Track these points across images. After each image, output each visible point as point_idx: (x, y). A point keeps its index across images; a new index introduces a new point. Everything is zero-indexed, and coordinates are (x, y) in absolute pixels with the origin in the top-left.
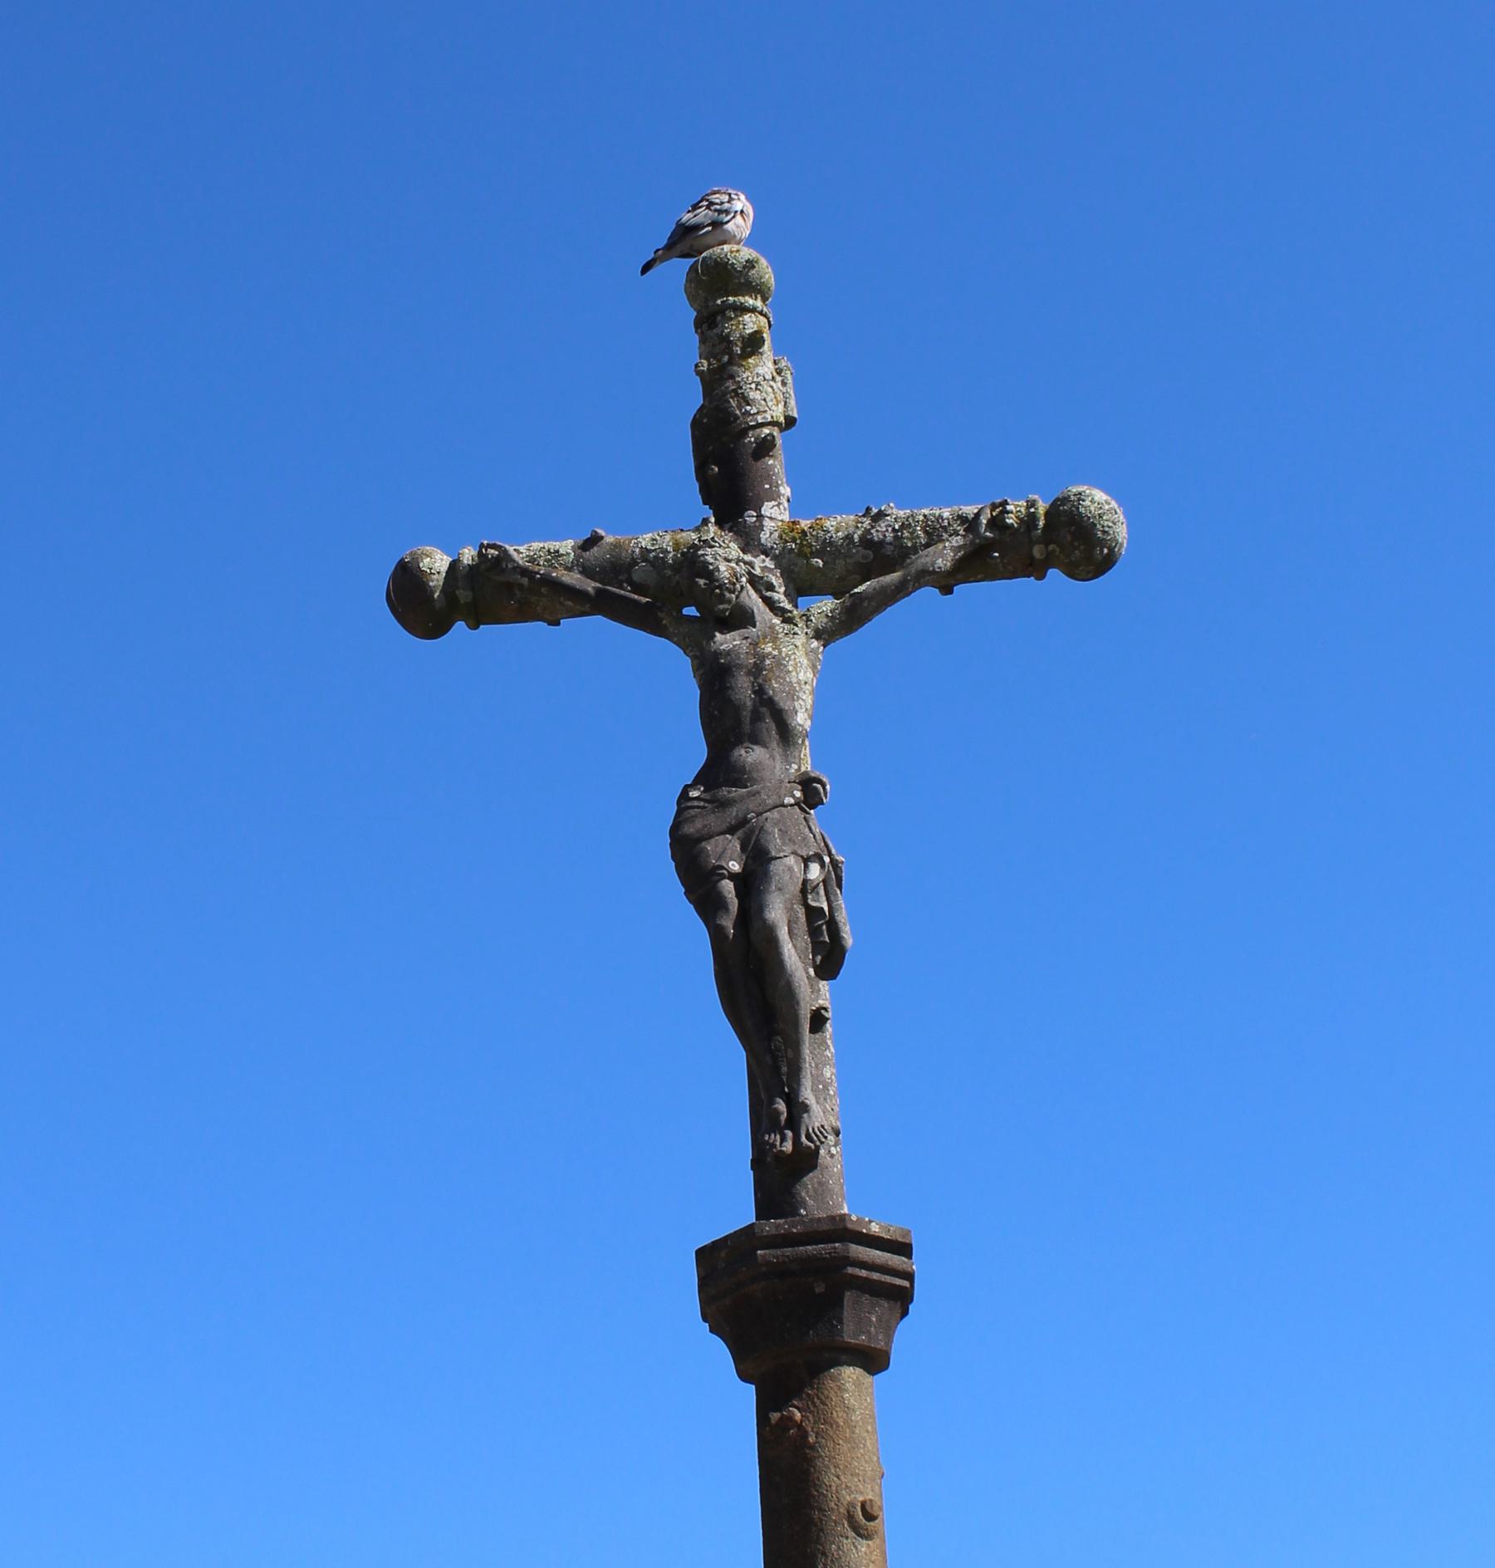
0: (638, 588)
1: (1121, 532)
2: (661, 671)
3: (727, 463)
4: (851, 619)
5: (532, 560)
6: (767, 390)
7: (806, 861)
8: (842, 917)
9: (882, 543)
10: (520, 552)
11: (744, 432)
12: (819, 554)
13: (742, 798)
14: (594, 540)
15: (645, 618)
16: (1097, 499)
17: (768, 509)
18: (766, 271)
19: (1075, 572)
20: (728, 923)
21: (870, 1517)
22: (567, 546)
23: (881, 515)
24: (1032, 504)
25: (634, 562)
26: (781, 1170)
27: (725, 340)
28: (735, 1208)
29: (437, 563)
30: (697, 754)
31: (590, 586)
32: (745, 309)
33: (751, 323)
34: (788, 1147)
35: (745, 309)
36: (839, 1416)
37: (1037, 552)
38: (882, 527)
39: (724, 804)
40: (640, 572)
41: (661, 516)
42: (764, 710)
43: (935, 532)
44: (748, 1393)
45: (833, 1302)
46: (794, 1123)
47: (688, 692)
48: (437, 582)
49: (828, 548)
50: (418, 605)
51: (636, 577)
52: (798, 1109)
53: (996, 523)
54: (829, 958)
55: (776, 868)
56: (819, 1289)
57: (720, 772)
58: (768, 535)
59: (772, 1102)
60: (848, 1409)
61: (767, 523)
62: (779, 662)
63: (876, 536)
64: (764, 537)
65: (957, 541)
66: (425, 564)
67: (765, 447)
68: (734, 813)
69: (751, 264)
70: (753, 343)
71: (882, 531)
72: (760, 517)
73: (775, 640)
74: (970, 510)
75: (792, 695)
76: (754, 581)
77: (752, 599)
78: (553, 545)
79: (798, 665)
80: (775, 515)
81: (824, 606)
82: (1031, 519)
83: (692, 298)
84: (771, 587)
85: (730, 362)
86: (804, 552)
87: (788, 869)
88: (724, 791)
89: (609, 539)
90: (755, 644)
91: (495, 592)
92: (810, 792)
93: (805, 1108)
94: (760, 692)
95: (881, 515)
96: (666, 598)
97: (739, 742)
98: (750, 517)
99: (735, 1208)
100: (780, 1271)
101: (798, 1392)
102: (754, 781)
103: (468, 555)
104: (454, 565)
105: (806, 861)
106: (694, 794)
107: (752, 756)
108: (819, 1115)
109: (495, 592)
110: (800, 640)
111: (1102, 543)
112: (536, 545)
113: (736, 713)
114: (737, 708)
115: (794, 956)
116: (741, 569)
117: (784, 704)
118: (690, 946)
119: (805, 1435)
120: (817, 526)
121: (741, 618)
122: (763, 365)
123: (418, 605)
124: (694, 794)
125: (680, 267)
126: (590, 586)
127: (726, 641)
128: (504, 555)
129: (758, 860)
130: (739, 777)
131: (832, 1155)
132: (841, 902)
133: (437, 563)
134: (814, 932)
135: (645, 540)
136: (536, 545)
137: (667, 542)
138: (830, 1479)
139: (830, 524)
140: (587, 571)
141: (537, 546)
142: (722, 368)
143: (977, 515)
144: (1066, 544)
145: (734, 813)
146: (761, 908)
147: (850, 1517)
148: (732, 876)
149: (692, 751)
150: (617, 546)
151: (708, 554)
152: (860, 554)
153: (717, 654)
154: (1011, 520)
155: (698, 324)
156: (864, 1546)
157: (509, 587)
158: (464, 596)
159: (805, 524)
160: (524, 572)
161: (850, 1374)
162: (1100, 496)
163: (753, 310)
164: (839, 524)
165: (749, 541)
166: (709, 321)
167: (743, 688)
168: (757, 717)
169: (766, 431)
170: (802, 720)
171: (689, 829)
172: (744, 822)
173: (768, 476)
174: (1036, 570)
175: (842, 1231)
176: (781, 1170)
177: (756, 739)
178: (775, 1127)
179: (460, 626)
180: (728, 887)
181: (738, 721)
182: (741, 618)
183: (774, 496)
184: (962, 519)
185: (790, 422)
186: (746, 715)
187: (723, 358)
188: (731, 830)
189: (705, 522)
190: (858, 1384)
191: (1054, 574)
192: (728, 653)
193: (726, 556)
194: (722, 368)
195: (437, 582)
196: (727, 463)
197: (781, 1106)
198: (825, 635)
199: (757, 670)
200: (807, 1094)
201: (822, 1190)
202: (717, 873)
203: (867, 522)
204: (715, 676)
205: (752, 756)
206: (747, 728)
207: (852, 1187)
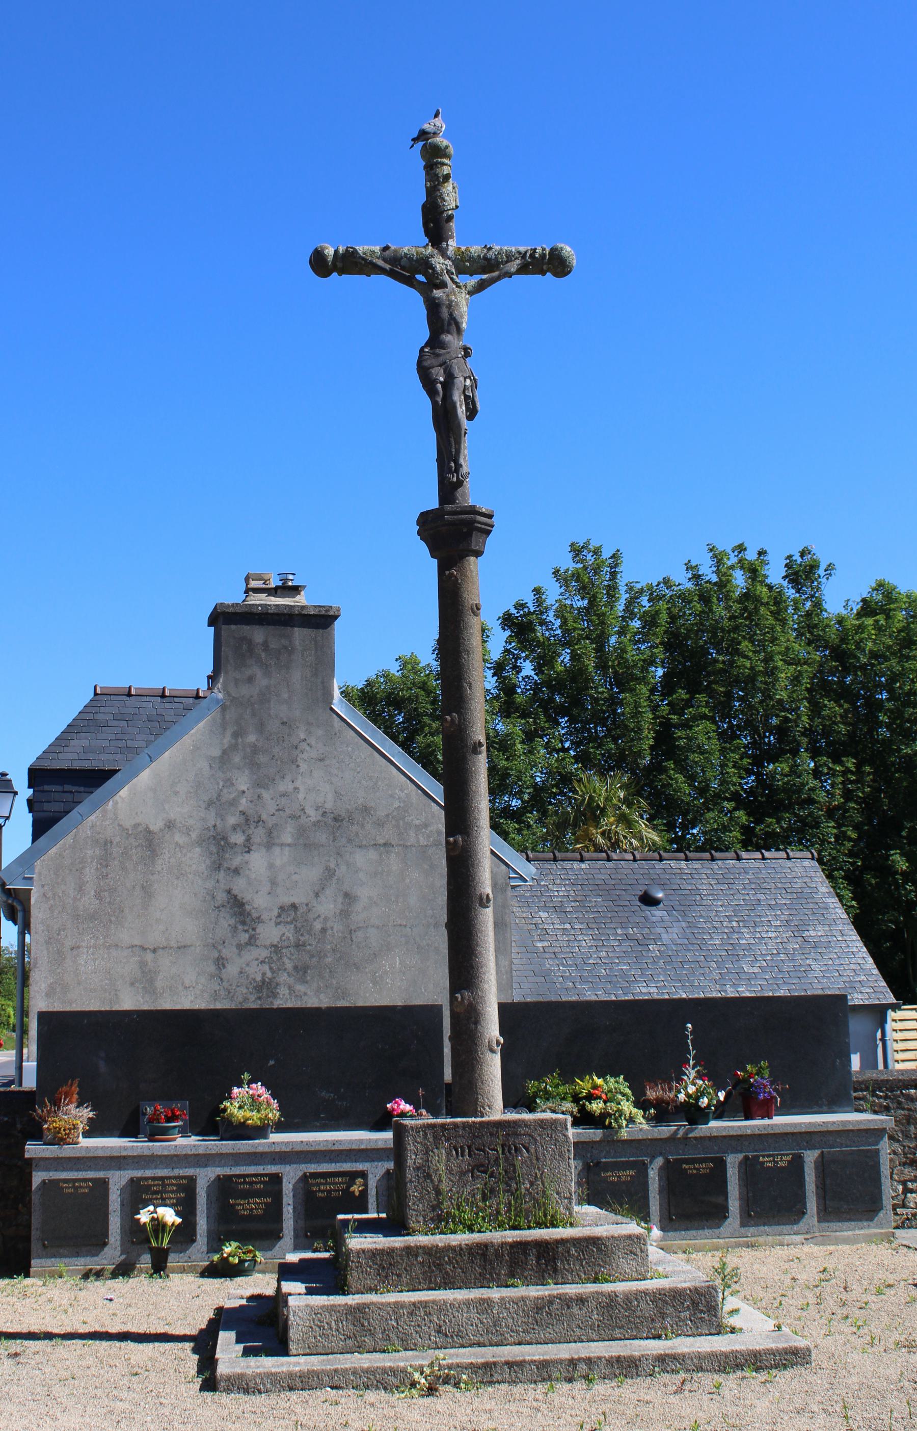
0: (403, 268)
1: (574, 263)
2: (411, 303)
3: (435, 222)
4: (481, 286)
5: (365, 254)
6: (451, 195)
7: (465, 378)
8: (477, 399)
9: (490, 259)
10: (360, 249)
11: (443, 212)
12: (468, 261)
13: (444, 354)
14: (386, 248)
15: (409, 281)
16: (568, 250)
17: (450, 242)
18: (451, 150)
19: (557, 274)
20: (439, 400)
21: (478, 609)
22: (377, 249)
23: (490, 249)
24: (544, 249)
25: (402, 258)
26: (449, 487)
27: (437, 175)
28: (432, 502)
29: (330, 252)
30: (425, 335)
31: (388, 267)
32: (443, 164)
33: (446, 170)
34: (455, 479)
35: (443, 164)
36: (469, 574)
37: (545, 267)
38: (491, 253)
39: (438, 355)
40: (404, 262)
41: (412, 241)
42: (452, 322)
43: (510, 257)
44: (10, 922)
45: (469, 535)
46: (457, 471)
47: (422, 312)
48: (330, 259)
49: (471, 259)
50: (320, 265)
51: (402, 263)
52: (458, 466)
53: (532, 256)
54: (472, 413)
55: (456, 380)
56: (465, 530)
57: (435, 342)
58: (450, 252)
59: (449, 463)
60: (472, 572)
61: (450, 248)
62: (457, 304)
63: (489, 256)
64: (449, 253)
65: (518, 262)
66: (326, 252)
67: (450, 218)
68: (441, 359)
69: (447, 147)
70: (447, 178)
71: (491, 255)
72: (447, 245)
73: (455, 294)
74: (522, 249)
75: (462, 317)
76: (448, 272)
77: (447, 278)
78: (373, 248)
79: (464, 305)
80: (452, 244)
81: (472, 281)
82: (545, 255)
83: (423, 157)
84: (453, 274)
85: (438, 184)
86: (463, 260)
87: (460, 381)
88: (437, 350)
89: (393, 247)
90: (448, 296)
91: (350, 263)
92: (467, 352)
93: (461, 466)
94: (451, 315)
95: (490, 249)
96: (405, 269)
97: (443, 332)
98: (444, 245)
99: (432, 502)
100: (452, 523)
101: (455, 565)
102: (448, 348)
103: (341, 250)
104: (336, 252)
105: (465, 378)
106: (426, 350)
107: (447, 338)
108: (465, 469)
109: (350, 263)
110: (463, 295)
111: (568, 266)
112: (366, 247)
113: (441, 322)
114: (443, 320)
115: (461, 411)
116: (444, 267)
117: (459, 320)
118: (424, 406)
119: (457, 580)
120: (467, 250)
121: (443, 285)
122: (449, 187)
123: (320, 265)
124: (426, 350)
125: (421, 144)
126: (388, 267)
127: (437, 293)
128: (355, 251)
129: (450, 378)
130: (443, 345)
131: (468, 483)
132: (477, 393)
133: (330, 252)
134: (467, 404)
135: (405, 250)
136: (366, 247)
137: (413, 251)
138: (465, 595)
139: (472, 250)
140: (385, 260)
141: (367, 248)
142: (435, 186)
143: (526, 252)
144: (554, 264)
145: (441, 359)
146: (451, 396)
147: (472, 609)
148: (441, 383)
149: (424, 334)
150: (395, 251)
151: (433, 261)
152: (483, 262)
153: (435, 298)
154: (537, 256)
155: (425, 167)
156: (476, 619)
157: (356, 263)
158: (339, 265)
159: (463, 248)
160: (363, 259)
161: (472, 559)
162: (568, 249)
163: (447, 165)
164: (476, 250)
165: (443, 253)
166: (431, 168)
167: (445, 313)
168: (449, 324)
169: (450, 212)
170: (464, 325)
171: (426, 364)
172: (445, 363)
173: (450, 230)
174: (543, 273)
175: (473, 511)
176: (449, 487)
177: (449, 332)
178: (450, 472)
179: (335, 274)
180: (439, 386)
181: (443, 325)
182: (443, 285)
183: (452, 237)
184: (519, 253)
185: (457, 207)
186: (446, 323)
187: (435, 182)
188: (441, 366)
189: (427, 245)
190: (474, 562)
191: (548, 274)
192: (439, 298)
193: (439, 263)
194: (435, 186)
195: (330, 259)
196: (435, 222)
197: (453, 464)
198: (470, 293)
199: (449, 306)
200: (462, 461)
201: (464, 495)
202: (435, 381)
203: (485, 251)
204: (433, 308)
205: (447, 338)
206: (446, 327)
207: (474, 494)
